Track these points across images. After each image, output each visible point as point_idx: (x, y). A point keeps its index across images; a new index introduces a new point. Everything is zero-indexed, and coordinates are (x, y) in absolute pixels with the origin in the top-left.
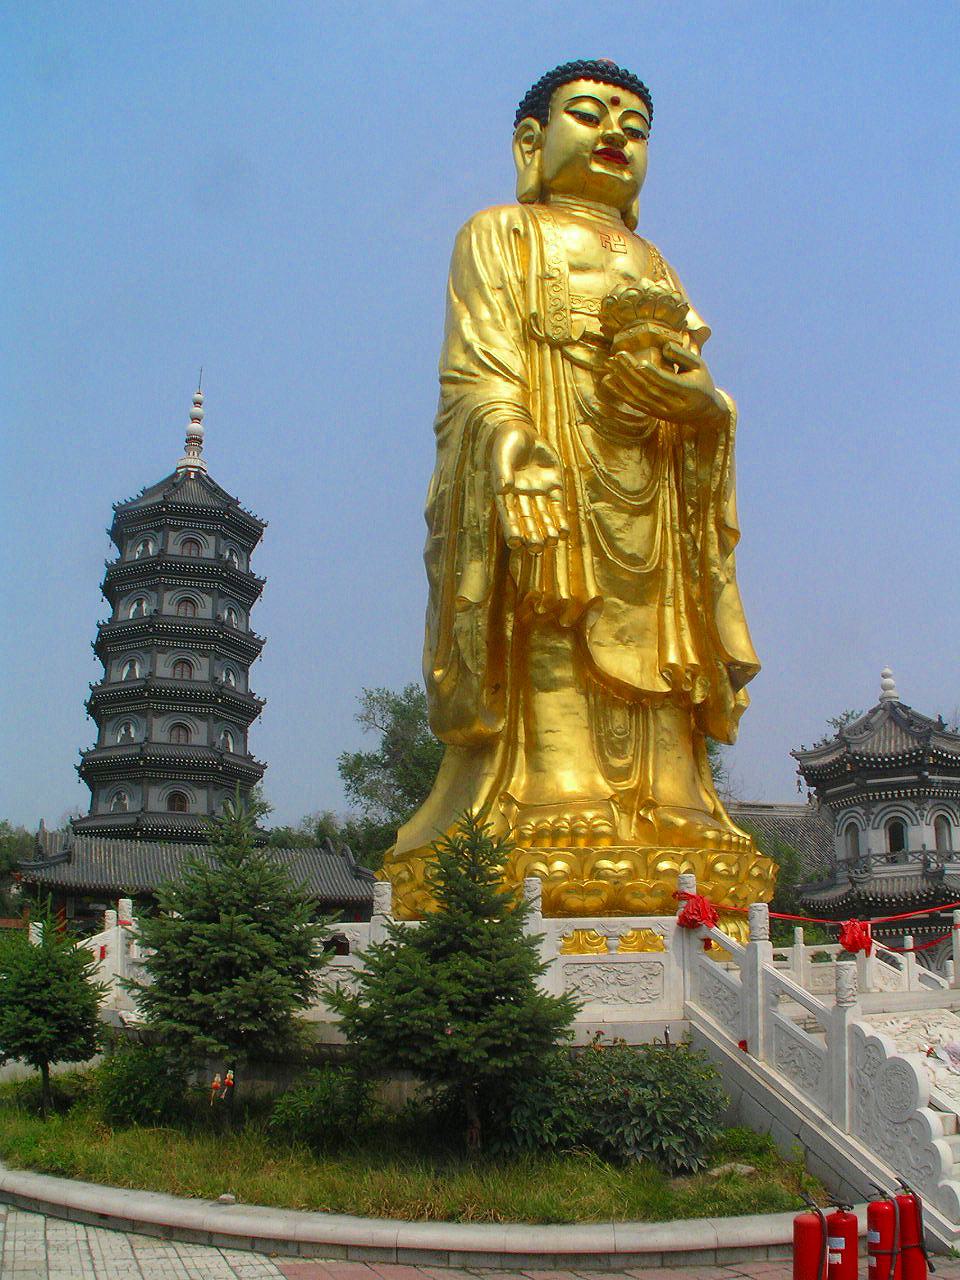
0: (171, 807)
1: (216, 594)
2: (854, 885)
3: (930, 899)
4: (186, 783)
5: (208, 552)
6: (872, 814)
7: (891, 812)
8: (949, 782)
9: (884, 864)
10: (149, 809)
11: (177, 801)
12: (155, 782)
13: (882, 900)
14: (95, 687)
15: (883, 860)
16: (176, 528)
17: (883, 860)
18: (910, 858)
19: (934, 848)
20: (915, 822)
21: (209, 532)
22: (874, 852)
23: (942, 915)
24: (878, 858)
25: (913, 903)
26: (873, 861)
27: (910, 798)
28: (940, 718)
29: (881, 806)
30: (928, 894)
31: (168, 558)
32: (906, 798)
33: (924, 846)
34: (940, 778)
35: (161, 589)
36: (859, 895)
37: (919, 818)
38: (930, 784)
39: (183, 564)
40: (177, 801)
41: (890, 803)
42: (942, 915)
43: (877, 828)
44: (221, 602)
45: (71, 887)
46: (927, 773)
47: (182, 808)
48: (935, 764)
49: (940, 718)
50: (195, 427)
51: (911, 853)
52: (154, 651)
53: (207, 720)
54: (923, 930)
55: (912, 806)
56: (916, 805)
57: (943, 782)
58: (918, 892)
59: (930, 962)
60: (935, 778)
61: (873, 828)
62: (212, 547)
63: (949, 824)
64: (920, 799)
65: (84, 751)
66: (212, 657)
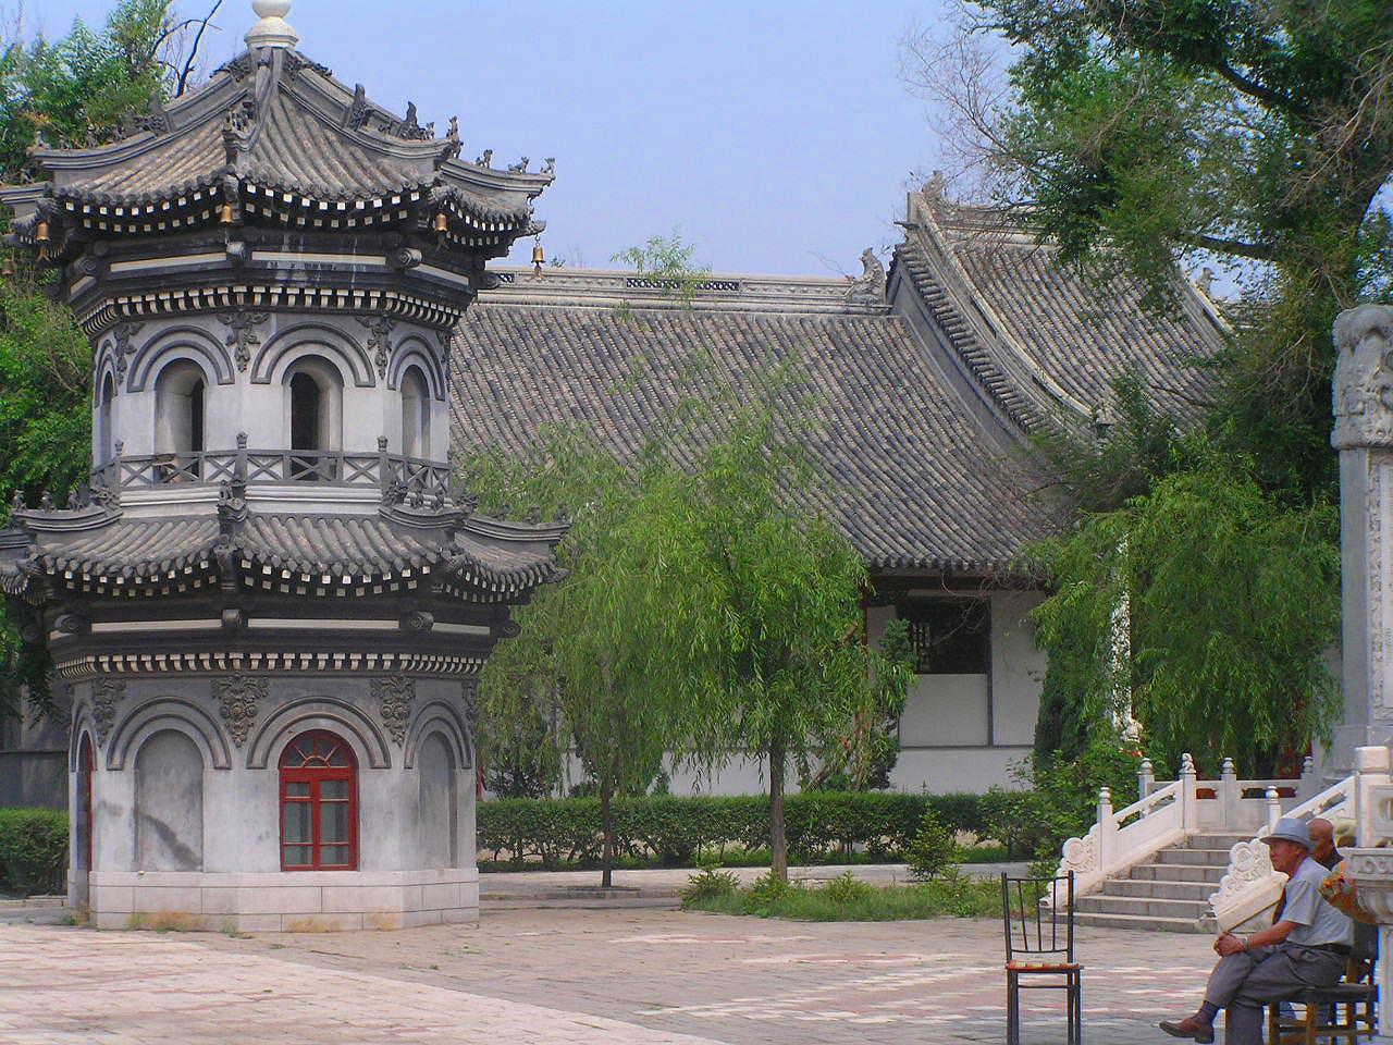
6: (255, 343)
7: (161, 353)
8: (328, 270)
9: (277, 481)
13: (396, 575)
15: (278, 469)
17: (278, 469)
18: (348, 471)
20: (226, 377)
22: (128, 452)
23: (438, 627)
24: (136, 468)
25: (94, 589)
26: (125, 475)
27: (357, 314)
28: (412, 110)
29: (150, 330)
32: (205, 311)
33: (241, 439)
34: (301, 258)
36: (237, 558)
37: (376, 370)
38: (266, 275)
41: (170, 324)
42: (438, 627)
43: (141, 389)
46: (416, 254)
49: (412, 110)
55: (220, 331)
56: (229, 331)
57: (310, 270)
59: (232, 747)
60: (283, 258)
61: (130, 390)
63: (425, 394)
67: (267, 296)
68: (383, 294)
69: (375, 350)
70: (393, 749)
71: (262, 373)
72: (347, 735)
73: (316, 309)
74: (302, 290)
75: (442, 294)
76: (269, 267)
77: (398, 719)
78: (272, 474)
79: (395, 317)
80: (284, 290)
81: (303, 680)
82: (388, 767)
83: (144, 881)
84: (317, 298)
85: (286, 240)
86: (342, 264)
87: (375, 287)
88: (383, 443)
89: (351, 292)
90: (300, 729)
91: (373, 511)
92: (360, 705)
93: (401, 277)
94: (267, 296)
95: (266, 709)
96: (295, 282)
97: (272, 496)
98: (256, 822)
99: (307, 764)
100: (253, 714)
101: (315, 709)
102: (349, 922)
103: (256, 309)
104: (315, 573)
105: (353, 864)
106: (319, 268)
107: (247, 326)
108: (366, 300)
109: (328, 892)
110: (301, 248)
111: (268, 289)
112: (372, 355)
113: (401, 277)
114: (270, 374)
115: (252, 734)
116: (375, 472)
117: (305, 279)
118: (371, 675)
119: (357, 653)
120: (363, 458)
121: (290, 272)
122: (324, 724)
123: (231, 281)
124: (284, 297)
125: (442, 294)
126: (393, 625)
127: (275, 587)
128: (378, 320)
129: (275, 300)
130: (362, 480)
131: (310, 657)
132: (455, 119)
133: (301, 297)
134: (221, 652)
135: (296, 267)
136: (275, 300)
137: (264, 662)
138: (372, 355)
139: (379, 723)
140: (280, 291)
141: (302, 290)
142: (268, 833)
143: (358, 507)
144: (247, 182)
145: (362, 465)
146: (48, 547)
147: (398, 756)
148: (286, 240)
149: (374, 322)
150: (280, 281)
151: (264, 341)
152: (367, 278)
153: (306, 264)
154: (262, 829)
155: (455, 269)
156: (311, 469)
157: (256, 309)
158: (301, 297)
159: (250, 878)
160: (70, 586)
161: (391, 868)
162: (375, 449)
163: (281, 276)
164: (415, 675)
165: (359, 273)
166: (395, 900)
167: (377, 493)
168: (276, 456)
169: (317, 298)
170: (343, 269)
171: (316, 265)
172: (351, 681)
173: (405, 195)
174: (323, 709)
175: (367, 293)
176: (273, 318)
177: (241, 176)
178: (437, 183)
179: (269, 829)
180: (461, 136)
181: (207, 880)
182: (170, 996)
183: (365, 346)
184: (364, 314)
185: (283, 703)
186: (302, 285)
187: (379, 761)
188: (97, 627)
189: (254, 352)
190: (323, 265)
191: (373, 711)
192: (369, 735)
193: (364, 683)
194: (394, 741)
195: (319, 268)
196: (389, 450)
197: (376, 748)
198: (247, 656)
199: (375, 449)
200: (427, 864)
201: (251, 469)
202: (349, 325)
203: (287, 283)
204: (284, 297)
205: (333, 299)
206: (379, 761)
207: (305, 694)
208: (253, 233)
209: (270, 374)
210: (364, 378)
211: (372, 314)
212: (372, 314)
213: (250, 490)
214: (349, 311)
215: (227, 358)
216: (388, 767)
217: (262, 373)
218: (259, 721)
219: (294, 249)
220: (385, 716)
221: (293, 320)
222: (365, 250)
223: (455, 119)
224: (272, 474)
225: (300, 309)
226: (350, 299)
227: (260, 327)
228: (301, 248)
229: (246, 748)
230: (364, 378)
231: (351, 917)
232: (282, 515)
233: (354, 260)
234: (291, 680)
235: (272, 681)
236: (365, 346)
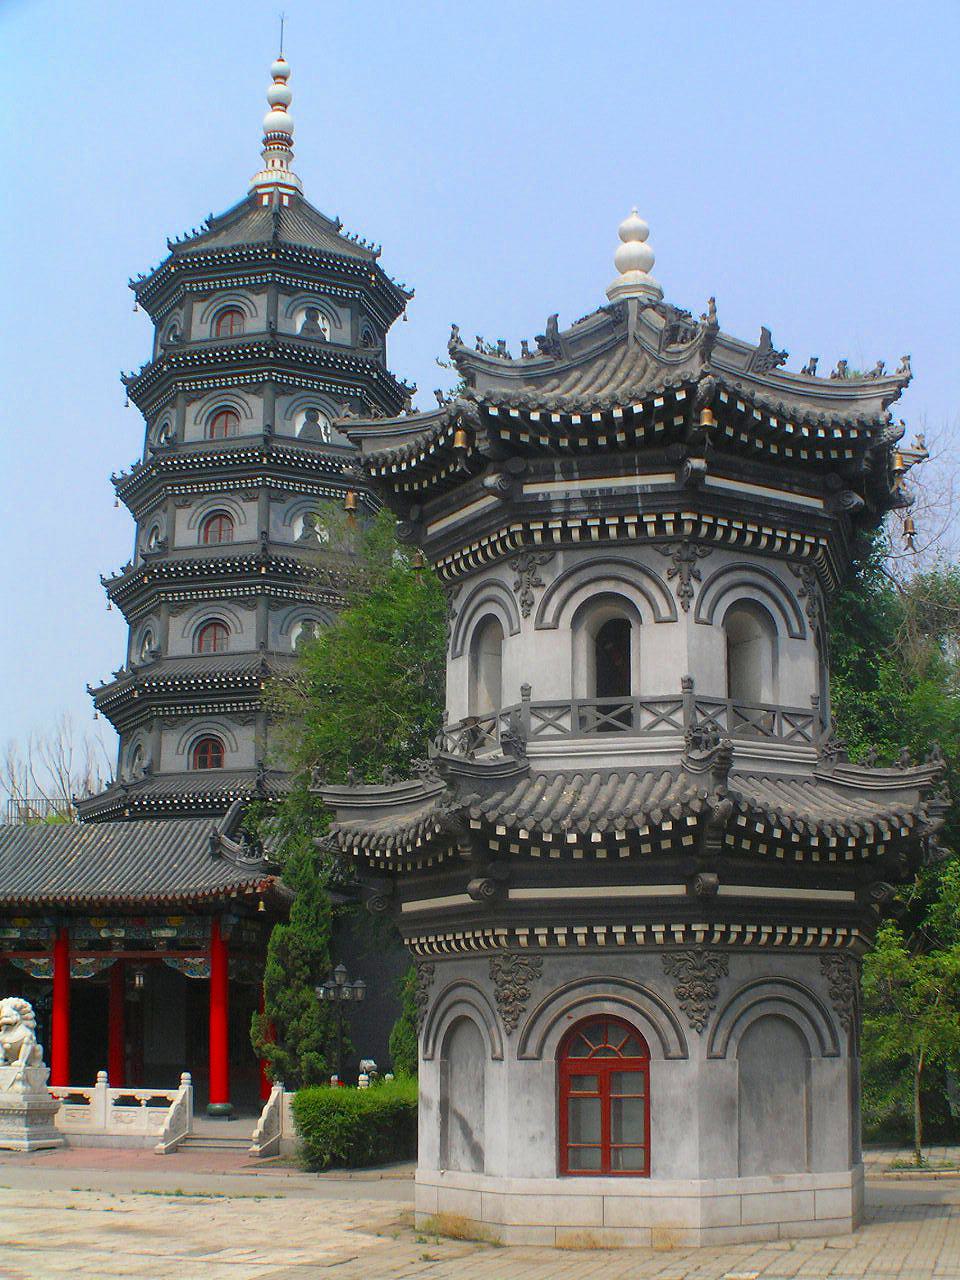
0: (203, 763)
1: (268, 390)
2: (127, 790)
3: (688, 841)
4: (221, 719)
5: (255, 323)
6: (539, 585)
8: (608, 495)
9: (565, 735)
10: (164, 769)
11: (208, 751)
12: (171, 722)
14: (110, 581)
15: (566, 722)
16: (205, 295)
17: (566, 722)
18: (646, 718)
19: (720, 692)
21: (257, 289)
30: (680, 825)
31: (193, 348)
34: (577, 486)
35: (180, 401)
37: (678, 602)
38: (541, 509)
39: (524, 343)
40: (208, 751)
42: (725, 890)
44: (282, 403)
45: (174, 901)
47: (218, 762)
48: (716, 433)
50: (275, 117)
51: (648, 704)
52: (171, 507)
53: (254, 607)
54: (669, 935)
56: (669, 563)
57: (588, 497)
58: (648, 821)
60: (557, 488)
62: (263, 313)
64: (528, 556)
65: (95, 686)
66: (263, 497)
67: (547, 533)
68: (678, 516)
69: (677, 580)
70: (691, 1036)
71: (549, 618)
72: (636, 1020)
73: (604, 542)
74: (584, 522)
75: (777, 517)
76: (541, 498)
77: (701, 998)
78: (558, 728)
79: (709, 544)
80: (564, 524)
81: (583, 958)
82: (685, 1057)
83: (445, 1181)
84: (603, 529)
85: (557, 467)
86: (623, 488)
87: (667, 509)
88: (688, 683)
89: (640, 518)
90: (580, 1014)
91: (673, 761)
92: (651, 985)
93: (692, 493)
94: (547, 533)
95: (539, 992)
96: (574, 513)
97: (556, 752)
98: (528, 1120)
99: (593, 1055)
100: (524, 998)
101: (600, 990)
102: (635, 1238)
103: (538, 549)
104: (557, 831)
105: (646, 1172)
106: (598, 494)
107: (530, 569)
108: (660, 525)
109: (612, 1203)
110: (576, 475)
111: (546, 525)
112: (673, 586)
113: (692, 493)
114: (557, 618)
115: (524, 1021)
116: (679, 717)
117: (585, 508)
118: (659, 950)
119: (582, 925)
120: (663, 702)
121: (567, 501)
122: (609, 1008)
123: (506, 521)
124: (566, 531)
125: (777, 517)
126: (679, 890)
127: (635, 851)
128: (679, 546)
129: (557, 536)
130: (663, 727)
131: (585, 930)
132: (909, 358)
133: (585, 530)
134: (561, 926)
135: (571, 496)
136: (557, 536)
137: (533, 938)
138: (673, 586)
139: (674, 1005)
140: (559, 525)
141: (584, 522)
142: (542, 1133)
143: (656, 758)
144: (488, 404)
145: (662, 710)
146: (344, 824)
147: (697, 1045)
148: (557, 467)
149: (674, 549)
150: (558, 514)
151: (549, 581)
152: (656, 499)
153: (582, 492)
154: (536, 1128)
155: (796, 488)
156: (609, 718)
157: (538, 549)
158: (585, 530)
159: (520, 1184)
160: (578, 854)
161: (680, 1179)
162: (677, 690)
163: (558, 508)
164: (726, 949)
165: (644, 495)
166: (693, 1216)
167: (680, 741)
168: (563, 708)
169: (603, 529)
170: (625, 492)
171: (593, 491)
172: (641, 958)
173: (669, 395)
174: (609, 991)
175: (659, 517)
176: (560, 557)
177: (479, 398)
178: (704, 375)
179: (543, 1128)
180: (915, 371)
181: (487, 1184)
182: (753, 1227)
183: (664, 577)
184: (660, 542)
185: (560, 984)
186: (584, 516)
187: (675, 1050)
188: (515, 894)
189: (538, 595)
190: (601, 490)
191: (667, 993)
192: (663, 1020)
193: (656, 959)
194: (692, 1027)
195: (598, 494)
196: (697, 692)
197: (672, 1036)
198: (512, 932)
199: (677, 690)
200: (715, 1175)
201: (536, 723)
202: (646, 556)
203: (567, 516)
204: (566, 531)
205: (622, 527)
206: (675, 1050)
207: (585, 973)
208: (517, 465)
209: (557, 618)
210: (665, 612)
211: (671, 541)
212: (671, 541)
213: (532, 747)
214: (642, 540)
215: (514, 600)
216: (685, 1057)
217: (549, 618)
218: (533, 1005)
219: (569, 478)
220: (680, 997)
221: (581, 557)
222: (648, 468)
223: (909, 358)
224: (558, 728)
225: (586, 542)
226: (641, 526)
227: (545, 568)
228: (576, 475)
229: (518, 1035)
230: (665, 612)
231: (637, 1232)
232: (568, 772)
233: (638, 481)
234: (566, 958)
235: (546, 960)
236: (664, 577)
